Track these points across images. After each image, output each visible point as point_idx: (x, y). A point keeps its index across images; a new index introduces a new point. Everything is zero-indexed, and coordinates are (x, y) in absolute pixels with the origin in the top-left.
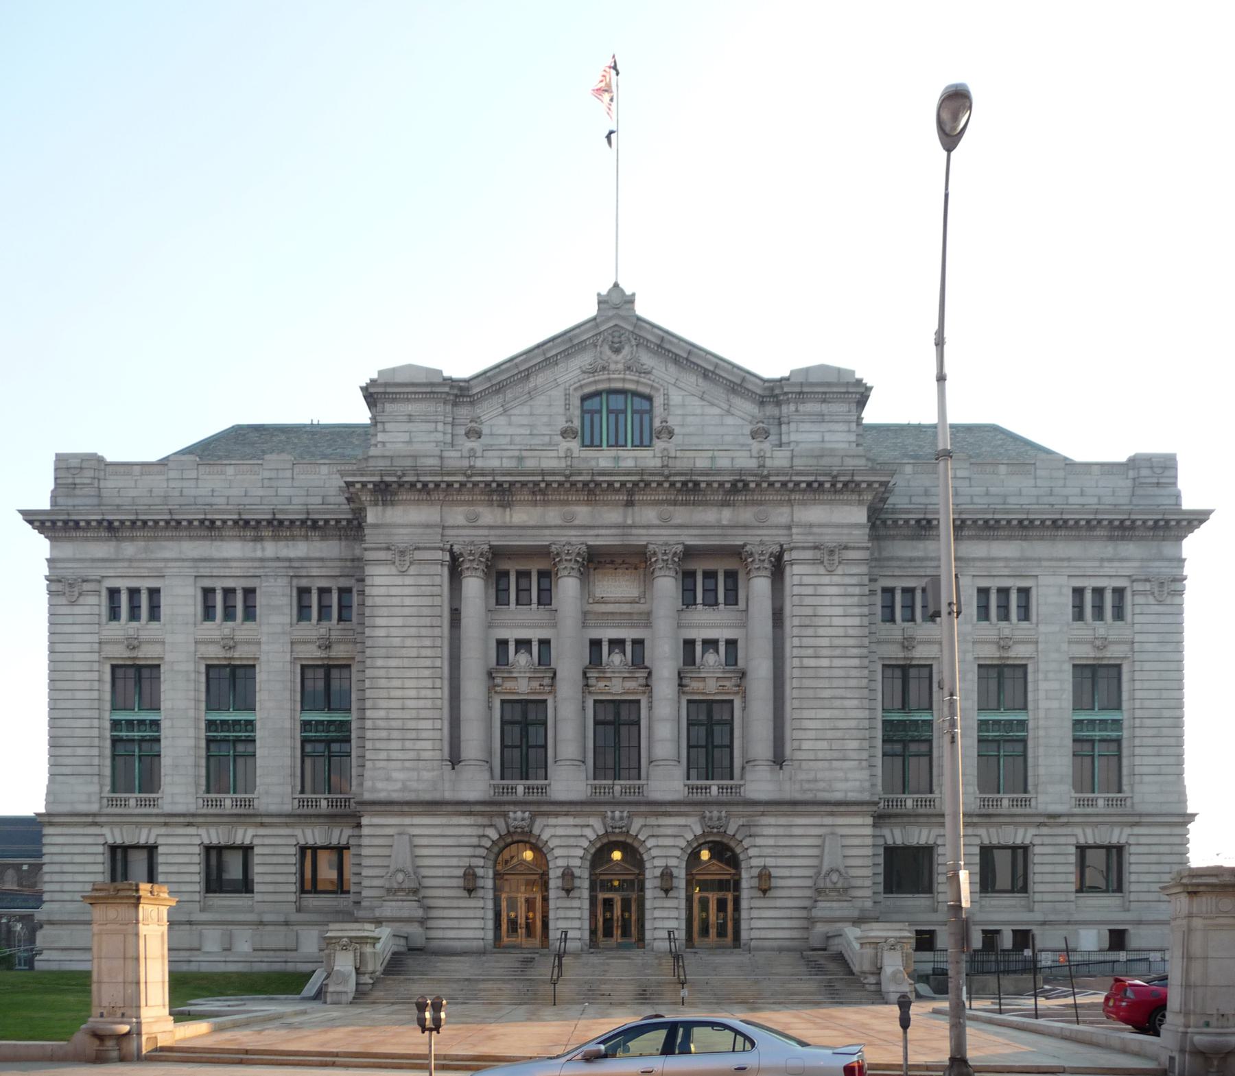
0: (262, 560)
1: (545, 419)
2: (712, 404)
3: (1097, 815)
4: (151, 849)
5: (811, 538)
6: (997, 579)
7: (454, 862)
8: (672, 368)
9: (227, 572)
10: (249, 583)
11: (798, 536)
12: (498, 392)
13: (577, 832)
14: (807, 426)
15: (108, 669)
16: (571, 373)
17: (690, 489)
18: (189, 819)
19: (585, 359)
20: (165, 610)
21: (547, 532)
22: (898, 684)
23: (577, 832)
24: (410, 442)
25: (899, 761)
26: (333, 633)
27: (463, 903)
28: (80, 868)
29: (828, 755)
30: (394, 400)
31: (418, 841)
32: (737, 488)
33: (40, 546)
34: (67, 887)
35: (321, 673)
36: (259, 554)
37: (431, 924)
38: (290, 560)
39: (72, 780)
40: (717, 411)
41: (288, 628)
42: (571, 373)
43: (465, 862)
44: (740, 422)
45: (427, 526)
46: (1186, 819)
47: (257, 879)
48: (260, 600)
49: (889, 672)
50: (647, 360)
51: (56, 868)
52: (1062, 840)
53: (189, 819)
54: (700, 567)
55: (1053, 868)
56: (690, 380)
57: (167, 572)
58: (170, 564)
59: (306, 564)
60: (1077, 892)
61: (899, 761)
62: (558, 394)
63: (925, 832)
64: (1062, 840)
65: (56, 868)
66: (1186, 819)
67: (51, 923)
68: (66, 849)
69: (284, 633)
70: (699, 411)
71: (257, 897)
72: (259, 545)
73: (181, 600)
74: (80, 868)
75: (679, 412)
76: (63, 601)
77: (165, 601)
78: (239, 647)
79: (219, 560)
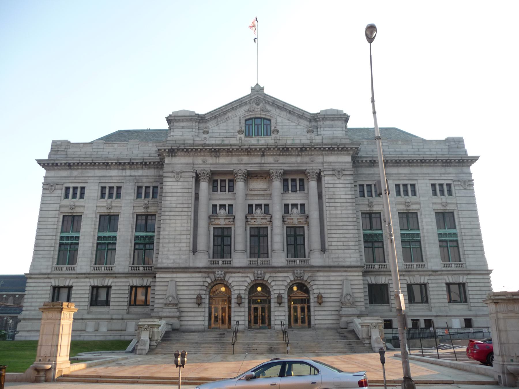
0: (125, 176)
1: (232, 127)
2: (292, 122)
3: (453, 271)
4: (70, 288)
5: (331, 167)
6: (402, 181)
7: (193, 292)
8: (278, 110)
9: (111, 181)
10: (119, 185)
11: (326, 166)
12: (215, 118)
13: (243, 279)
14: (327, 129)
15: (61, 217)
16: (242, 112)
17: (285, 150)
18: (86, 276)
19: (247, 108)
20: (86, 195)
21: (232, 166)
22: (368, 220)
23: (243, 279)
24: (183, 135)
25: (371, 250)
26: (113, 203)
27: (196, 310)
28: (40, 296)
29: (343, 248)
30: (177, 121)
31: (178, 284)
32: (303, 150)
33: (42, 172)
34: (33, 304)
35: (70, 218)
36: (124, 174)
37: (182, 319)
38: (135, 176)
39: (41, 260)
40: (294, 124)
41: (133, 201)
42: (242, 112)
43: (197, 292)
44: (303, 128)
45: (188, 164)
46: (489, 272)
47: (112, 300)
48: (123, 191)
49: (364, 216)
50: (269, 108)
51: (30, 296)
52: (440, 281)
53: (86, 276)
54: (290, 177)
55: (438, 293)
56: (284, 114)
57: (89, 181)
58: (90, 178)
59: (141, 178)
60: (449, 303)
61: (371, 250)
62: (237, 119)
63: (384, 278)
64: (440, 281)
65: (30, 296)
66: (489, 272)
67: (24, 319)
68: (35, 288)
69: (131, 203)
70: (288, 124)
71: (111, 308)
72: (124, 171)
73: (93, 191)
74: (40, 296)
75: (281, 124)
76: (48, 191)
77: (86, 191)
78: (113, 208)
79: (109, 177)
